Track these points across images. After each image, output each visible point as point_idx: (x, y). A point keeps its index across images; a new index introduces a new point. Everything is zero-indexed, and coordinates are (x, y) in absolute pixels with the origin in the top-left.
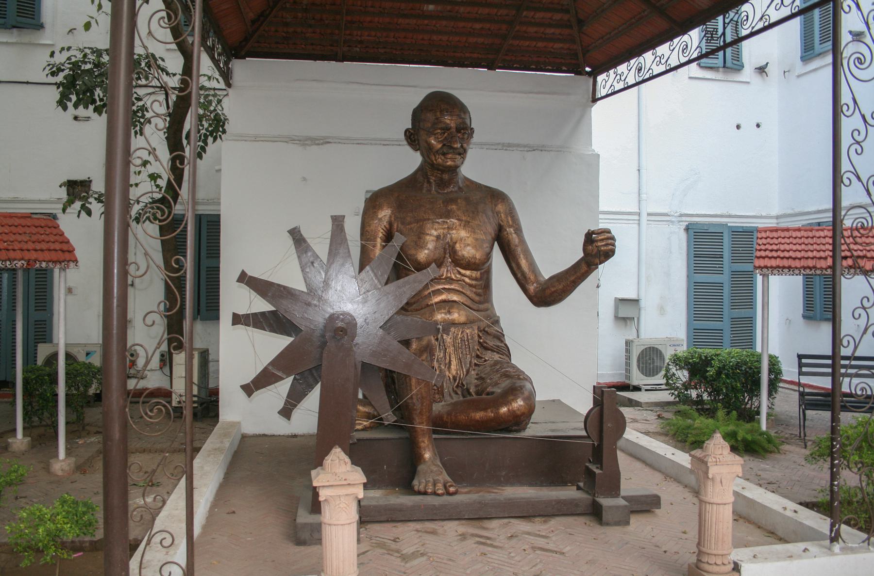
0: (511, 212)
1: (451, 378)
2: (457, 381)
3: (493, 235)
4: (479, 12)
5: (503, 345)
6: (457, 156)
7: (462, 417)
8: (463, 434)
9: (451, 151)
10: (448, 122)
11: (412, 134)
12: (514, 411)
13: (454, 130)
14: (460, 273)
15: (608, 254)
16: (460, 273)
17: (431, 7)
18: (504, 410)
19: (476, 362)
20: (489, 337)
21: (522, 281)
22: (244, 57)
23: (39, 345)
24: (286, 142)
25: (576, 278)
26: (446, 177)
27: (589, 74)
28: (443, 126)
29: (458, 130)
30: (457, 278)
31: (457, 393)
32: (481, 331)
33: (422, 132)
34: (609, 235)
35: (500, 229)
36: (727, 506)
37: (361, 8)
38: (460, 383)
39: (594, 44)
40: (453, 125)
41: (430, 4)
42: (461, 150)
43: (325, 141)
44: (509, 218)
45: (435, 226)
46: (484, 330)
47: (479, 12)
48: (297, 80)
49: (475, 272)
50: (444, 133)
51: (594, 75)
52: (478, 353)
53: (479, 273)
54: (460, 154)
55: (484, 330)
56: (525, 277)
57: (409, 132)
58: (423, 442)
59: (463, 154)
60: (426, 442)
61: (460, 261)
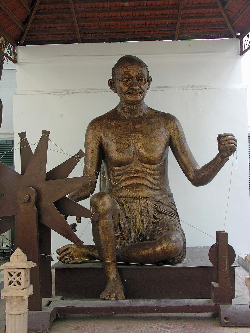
0: (177, 129)
1: (136, 231)
2: (140, 233)
3: (165, 142)
4: (158, 4)
5: (174, 211)
6: (138, 94)
7: (135, 254)
8: (129, 265)
9: (134, 91)
10: (131, 73)
11: (112, 83)
12: (165, 250)
13: (135, 78)
14: (144, 166)
15: (233, 150)
16: (144, 166)
17: (127, 4)
18: (158, 249)
19: (153, 221)
20: (163, 206)
21: (186, 170)
22: (24, 45)
23: (69, 225)
24: (50, 94)
25: (215, 167)
26: (135, 107)
27: (238, 37)
28: (128, 76)
29: (138, 78)
30: (142, 169)
31: (139, 240)
32: (157, 202)
33: (117, 81)
34: (232, 137)
35: (171, 138)
36: (27, 300)
37: (84, 9)
38: (142, 233)
39: (236, 17)
40: (134, 76)
41: (126, 1)
42: (141, 91)
43: (73, 91)
44: (176, 131)
45: (127, 139)
46: (159, 201)
47: (158, 4)
48: (55, 56)
49: (154, 165)
50: (129, 81)
51: (241, 37)
52: (155, 215)
53: (156, 166)
54: (140, 93)
55: (159, 201)
56: (187, 168)
57: (110, 82)
58: (109, 269)
59: (142, 93)
60: (111, 269)
61: (143, 159)
